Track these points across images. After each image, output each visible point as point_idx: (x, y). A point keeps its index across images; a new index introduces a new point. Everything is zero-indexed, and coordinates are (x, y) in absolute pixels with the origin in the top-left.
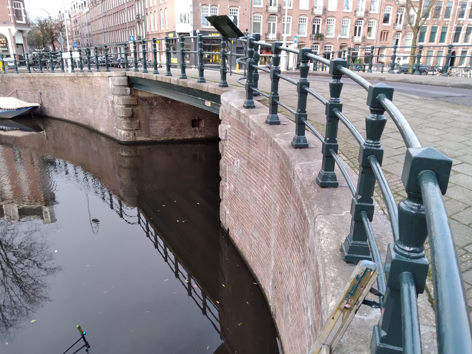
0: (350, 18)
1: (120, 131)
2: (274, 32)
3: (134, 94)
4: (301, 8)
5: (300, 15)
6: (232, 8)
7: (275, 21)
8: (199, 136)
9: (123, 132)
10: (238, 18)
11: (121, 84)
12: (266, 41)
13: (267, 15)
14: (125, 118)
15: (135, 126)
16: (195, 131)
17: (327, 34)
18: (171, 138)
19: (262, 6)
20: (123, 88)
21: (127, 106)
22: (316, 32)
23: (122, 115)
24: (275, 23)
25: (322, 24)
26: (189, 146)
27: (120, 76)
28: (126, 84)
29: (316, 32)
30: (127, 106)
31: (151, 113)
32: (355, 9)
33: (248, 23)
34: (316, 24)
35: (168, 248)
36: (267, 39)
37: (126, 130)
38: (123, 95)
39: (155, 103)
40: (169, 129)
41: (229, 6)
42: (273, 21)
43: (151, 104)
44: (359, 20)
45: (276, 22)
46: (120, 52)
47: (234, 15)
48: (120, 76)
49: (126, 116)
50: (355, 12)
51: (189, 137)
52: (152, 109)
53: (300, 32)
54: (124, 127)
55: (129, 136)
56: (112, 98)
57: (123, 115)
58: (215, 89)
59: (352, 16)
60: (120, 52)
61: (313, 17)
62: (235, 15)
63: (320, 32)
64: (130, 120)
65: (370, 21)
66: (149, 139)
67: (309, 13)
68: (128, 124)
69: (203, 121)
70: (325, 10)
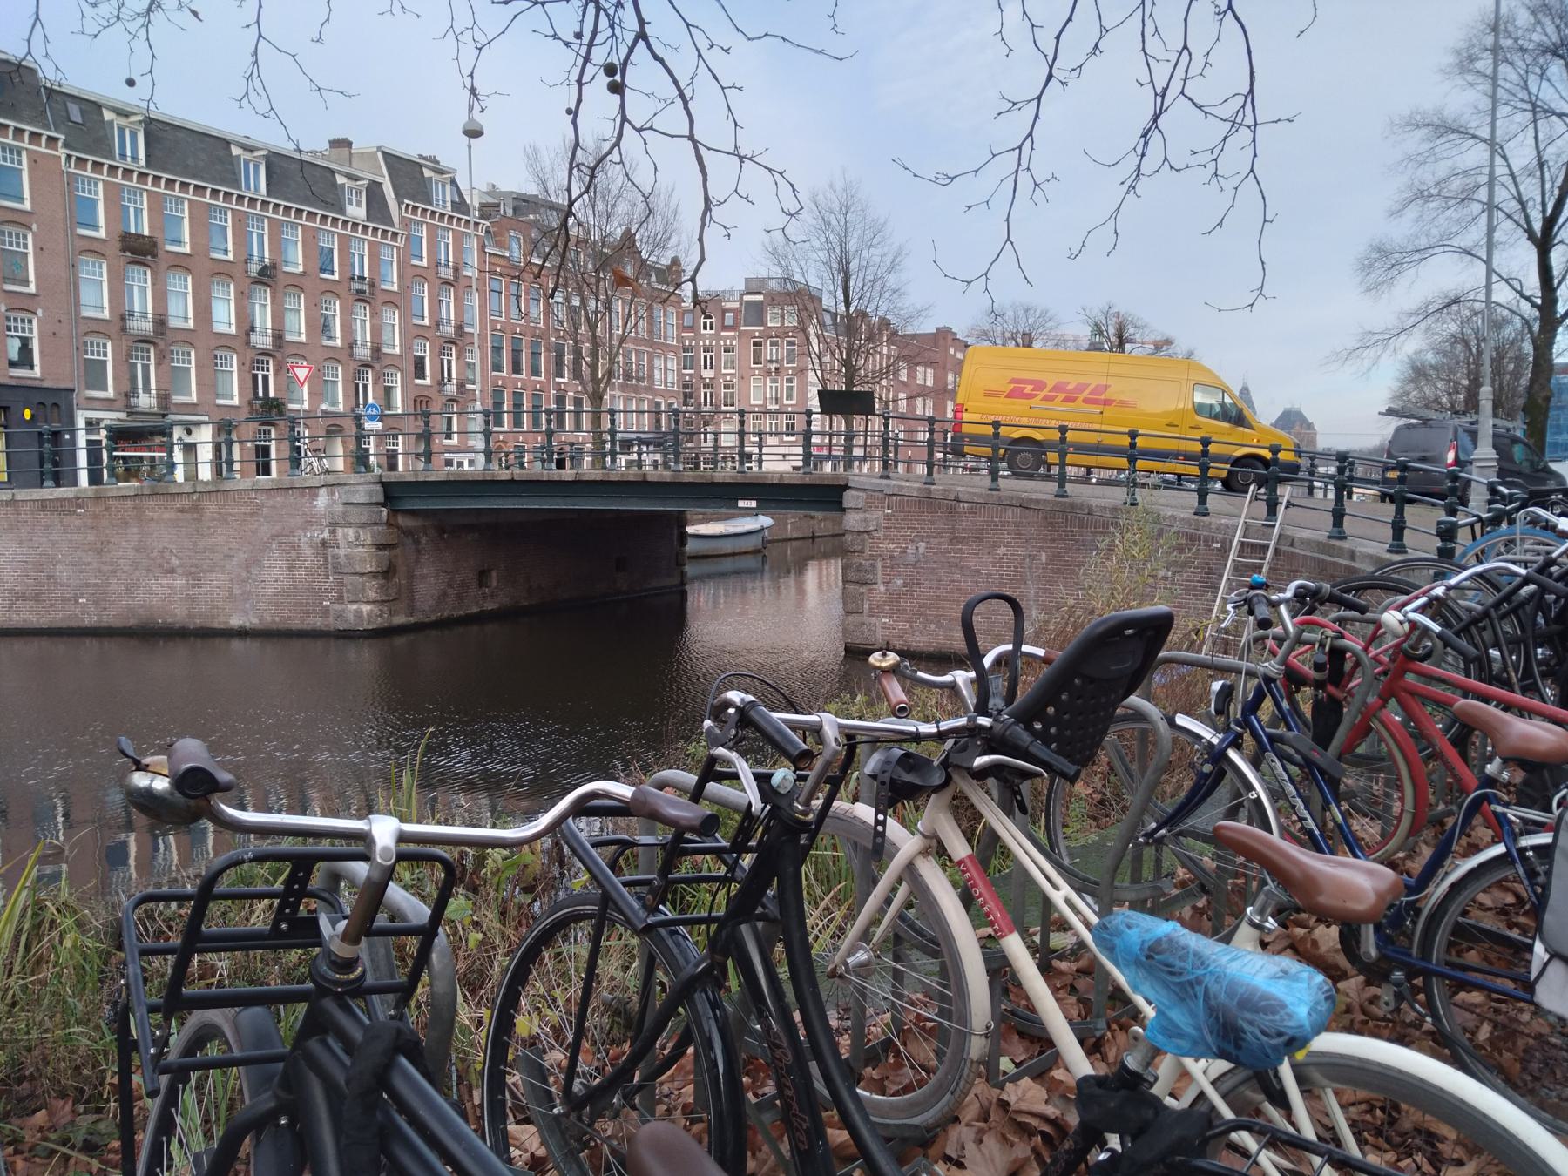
0: (340, 362)
1: (355, 607)
2: (147, 389)
3: (392, 521)
4: (87, 313)
5: (217, 348)
6: (12, 315)
7: (149, 359)
8: (490, 606)
9: (366, 608)
10: (36, 346)
11: (374, 500)
12: (129, 414)
13: (125, 343)
14: (374, 575)
15: (393, 591)
16: (484, 596)
17: (292, 401)
18: (446, 614)
19: (106, 314)
20: (376, 509)
21: (380, 547)
22: (261, 394)
23: (369, 568)
24: (148, 365)
25: (276, 374)
26: (434, 632)
27: (369, 483)
28: (381, 499)
29: (261, 394)
30: (380, 547)
31: (417, 561)
32: (351, 341)
33: (72, 362)
34: (260, 374)
35: (1555, 312)
36: (132, 407)
37: (374, 602)
38: (375, 524)
39: (424, 540)
40: (444, 594)
41: (3, 309)
42: (143, 359)
43: (417, 542)
44: (261, 358)
45: (152, 361)
46: (831, 427)
47: (20, 334)
48: (369, 483)
49: (379, 570)
50: (351, 347)
51: (475, 609)
52: (418, 551)
53: (220, 391)
54: (372, 595)
55: (381, 616)
56: (326, 534)
57: (373, 569)
58: (802, 479)
59: (344, 358)
60: (831, 427)
61: (250, 354)
62: (27, 335)
63: (272, 395)
64: (384, 578)
65: (386, 371)
66: (412, 620)
67: (114, 329)
68: (381, 587)
69: (494, 574)
70: (278, 337)
